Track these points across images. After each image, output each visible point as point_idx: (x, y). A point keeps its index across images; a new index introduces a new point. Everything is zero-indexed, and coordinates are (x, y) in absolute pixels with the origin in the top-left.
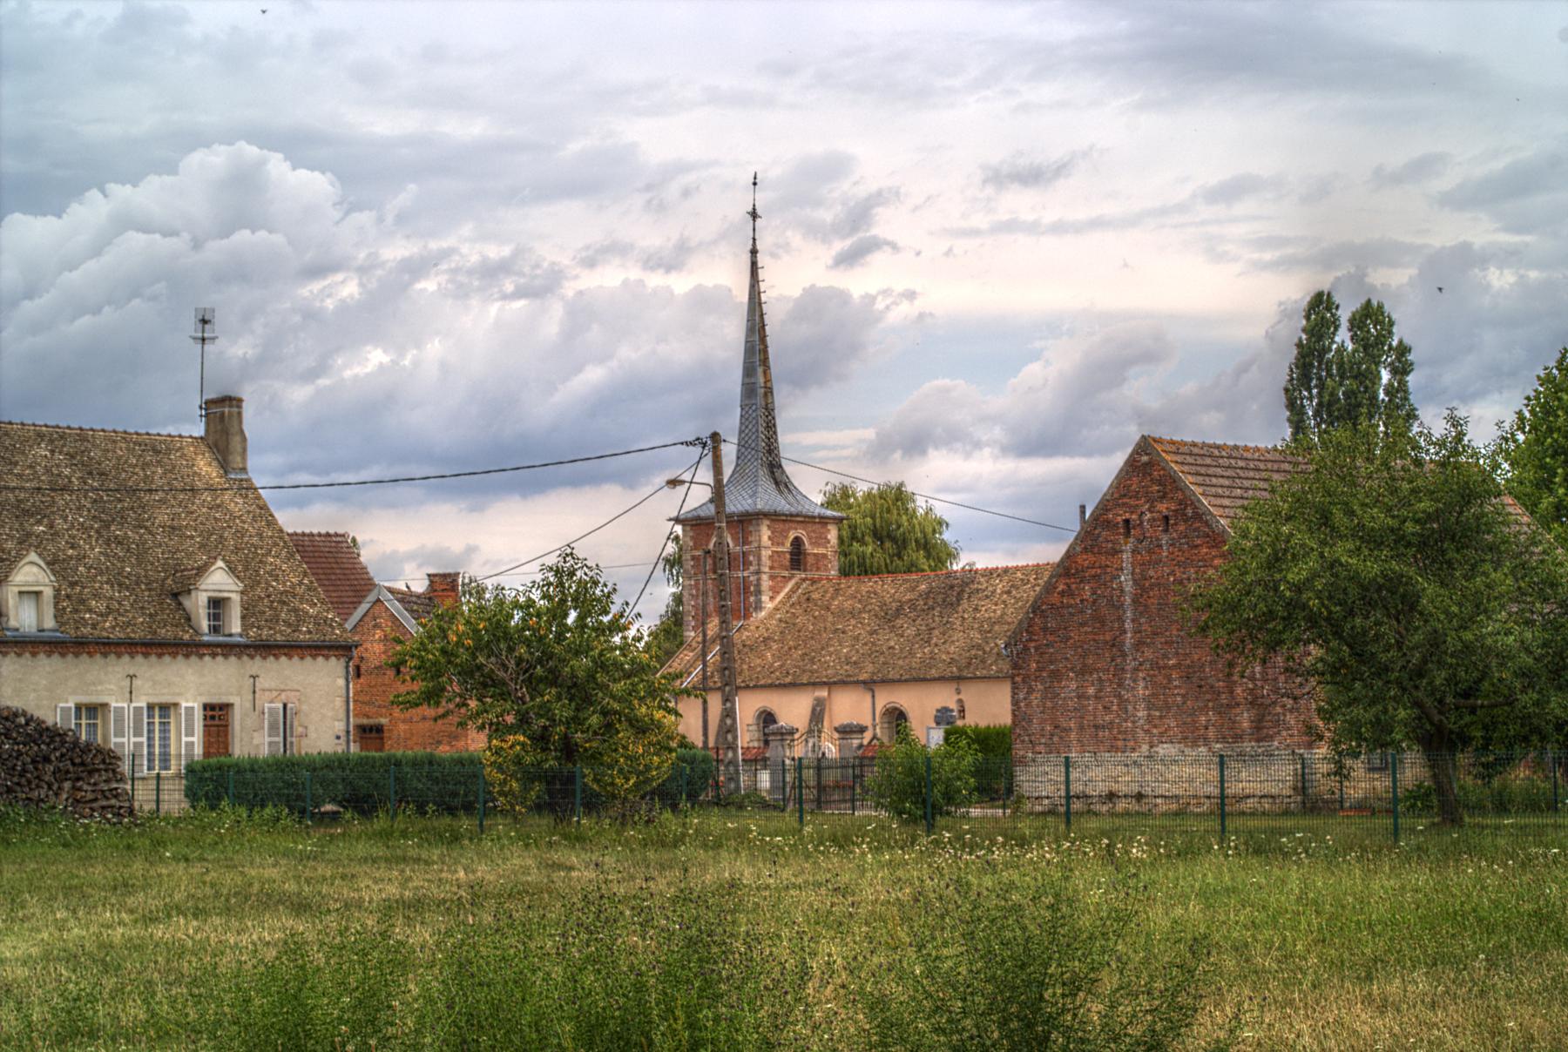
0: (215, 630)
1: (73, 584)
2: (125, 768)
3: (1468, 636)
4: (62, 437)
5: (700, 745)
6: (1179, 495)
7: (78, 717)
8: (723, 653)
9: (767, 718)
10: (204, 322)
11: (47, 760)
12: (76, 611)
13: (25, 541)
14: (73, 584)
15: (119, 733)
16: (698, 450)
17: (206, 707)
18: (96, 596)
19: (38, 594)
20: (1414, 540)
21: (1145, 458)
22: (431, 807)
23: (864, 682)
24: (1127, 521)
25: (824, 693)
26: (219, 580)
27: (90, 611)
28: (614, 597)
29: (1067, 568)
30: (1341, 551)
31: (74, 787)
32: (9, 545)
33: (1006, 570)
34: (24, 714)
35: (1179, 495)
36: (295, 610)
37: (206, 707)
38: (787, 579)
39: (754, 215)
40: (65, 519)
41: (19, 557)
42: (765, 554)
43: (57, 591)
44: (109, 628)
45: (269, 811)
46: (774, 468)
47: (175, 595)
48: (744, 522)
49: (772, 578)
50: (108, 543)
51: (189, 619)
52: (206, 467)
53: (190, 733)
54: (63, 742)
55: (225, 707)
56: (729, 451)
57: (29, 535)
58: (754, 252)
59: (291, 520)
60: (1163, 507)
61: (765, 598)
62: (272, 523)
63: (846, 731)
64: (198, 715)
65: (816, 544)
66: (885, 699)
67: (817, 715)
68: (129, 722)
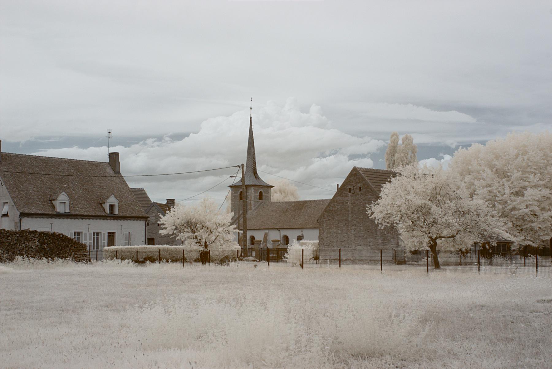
0: (111, 213)
1: (74, 201)
2: (88, 249)
3: (443, 220)
4: (71, 162)
5: (538, 257)
6: (364, 182)
7: (75, 235)
8: (244, 221)
9: (253, 238)
10: (109, 133)
11: (68, 246)
12: (74, 207)
13: (62, 189)
14: (74, 201)
15: (85, 240)
16: (238, 168)
17: (108, 233)
18: (80, 204)
19: (65, 203)
20: (429, 194)
21: (355, 172)
22: (170, 260)
23: (278, 229)
24: (350, 189)
25: (267, 231)
26: (112, 200)
27: (78, 207)
28: (387, 189)
29: (333, 200)
30: (410, 197)
31: (75, 254)
32: (57, 190)
33: (315, 201)
34: (62, 234)
35: (364, 182)
36: (132, 208)
37: (108, 233)
38: (258, 202)
39: (251, 108)
40: (72, 183)
41: (60, 193)
42: (253, 196)
43: (70, 202)
44: (83, 212)
45: (127, 260)
46: (255, 173)
47: (101, 204)
48: (248, 186)
49: (254, 201)
50: (83, 189)
51: (104, 210)
52: (109, 171)
53: (104, 240)
54: (72, 242)
55: (113, 233)
56: (245, 168)
57: (62, 187)
58: (251, 118)
59: (132, 185)
60: (359, 185)
61: (252, 207)
62: (127, 185)
63: (274, 241)
64: (107, 235)
65: (265, 193)
66: (284, 233)
67: (266, 236)
68: (88, 237)
